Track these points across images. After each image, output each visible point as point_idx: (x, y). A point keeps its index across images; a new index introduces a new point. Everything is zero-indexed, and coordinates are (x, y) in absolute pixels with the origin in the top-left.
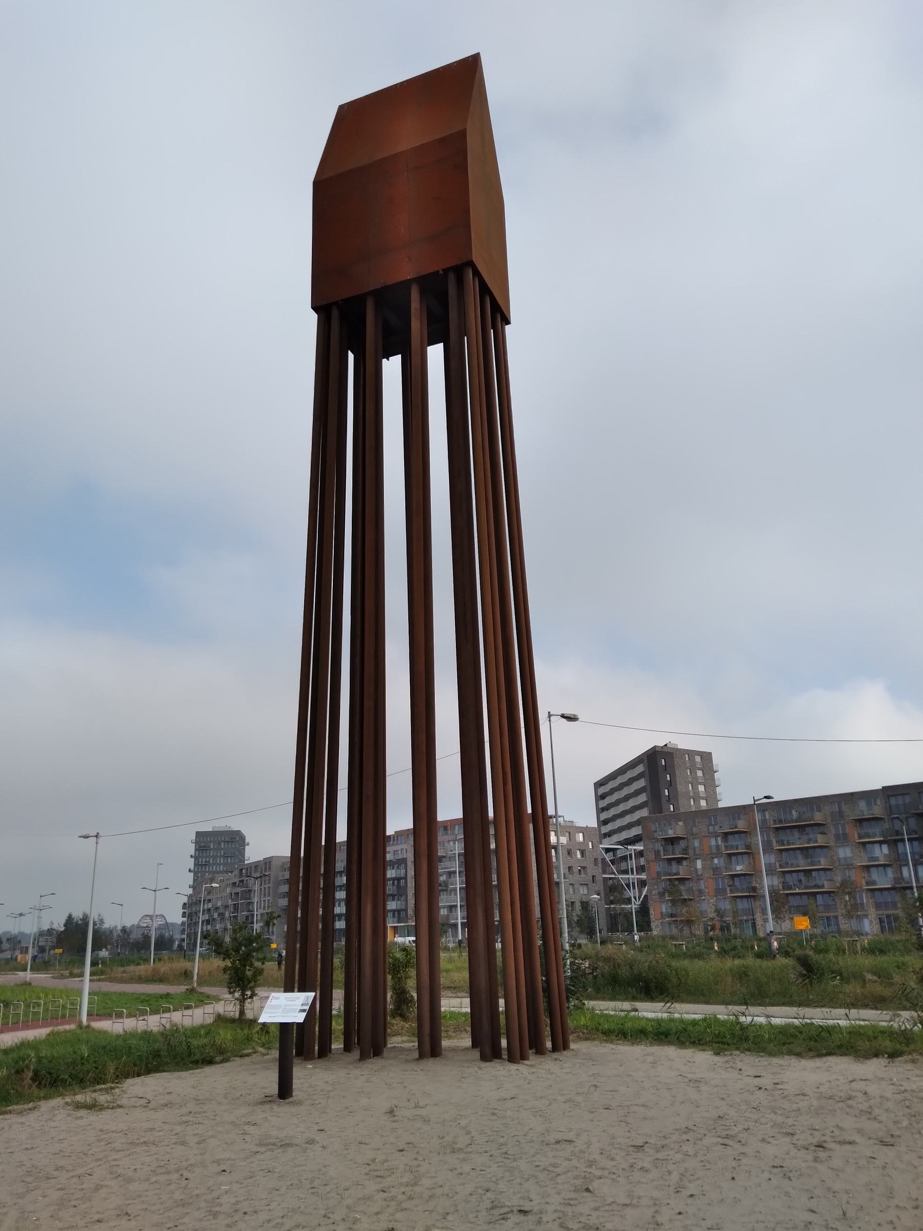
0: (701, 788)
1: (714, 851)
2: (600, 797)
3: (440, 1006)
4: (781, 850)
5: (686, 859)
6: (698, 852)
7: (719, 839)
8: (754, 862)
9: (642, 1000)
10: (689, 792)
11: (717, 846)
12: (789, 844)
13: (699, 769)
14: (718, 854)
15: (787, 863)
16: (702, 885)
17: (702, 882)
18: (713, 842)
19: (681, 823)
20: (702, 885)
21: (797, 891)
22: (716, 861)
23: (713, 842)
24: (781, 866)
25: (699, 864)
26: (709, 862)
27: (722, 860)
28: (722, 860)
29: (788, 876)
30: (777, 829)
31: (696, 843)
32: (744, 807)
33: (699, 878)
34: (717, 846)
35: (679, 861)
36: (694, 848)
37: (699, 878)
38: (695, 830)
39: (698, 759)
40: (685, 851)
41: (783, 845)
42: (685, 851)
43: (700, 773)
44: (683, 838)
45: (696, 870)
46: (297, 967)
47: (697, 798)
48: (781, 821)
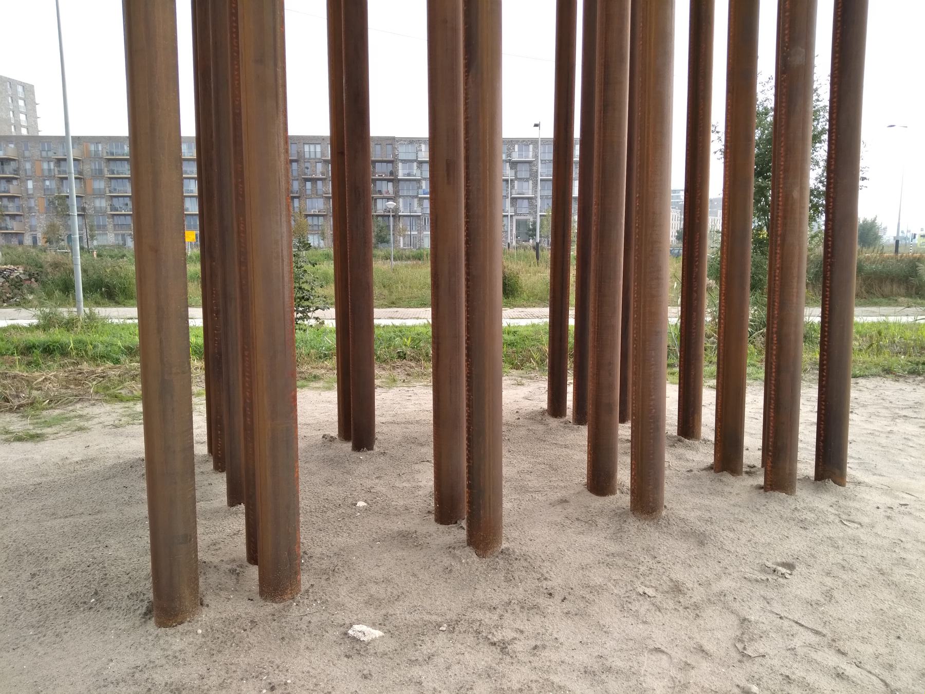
0: (23, 117)
1: (46, 173)
2: (24, 86)
3: (338, 374)
4: (111, 178)
5: (16, 179)
6: (29, 173)
7: (52, 165)
8: (85, 186)
9: (104, 305)
10: (10, 119)
11: (50, 170)
12: (118, 173)
13: (21, 99)
14: (51, 177)
15: (115, 190)
16: (32, 203)
17: (32, 201)
18: (45, 166)
19: (12, 146)
20: (32, 203)
21: (123, 212)
22: (47, 183)
23: (45, 166)
24: (110, 192)
25: (30, 184)
26: (41, 183)
27: (54, 183)
28: (54, 183)
29: (115, 200)
30: (109, 160)
31: (28, 166)
32: (59, 137)
33: (29, 197)
34: (50, 170)
35: (9, 180)
36: (26, 170)
37: (29, 197)
38: (27, 154)
39: (20, 89)
40: (16, 171)
41: (113, 173)
42: (16, 171)
43: (21, 103)
44: (14, 160)
45: (27, 189)
46: (572, 322)
47: (18, 126)
48: (112, 154)
